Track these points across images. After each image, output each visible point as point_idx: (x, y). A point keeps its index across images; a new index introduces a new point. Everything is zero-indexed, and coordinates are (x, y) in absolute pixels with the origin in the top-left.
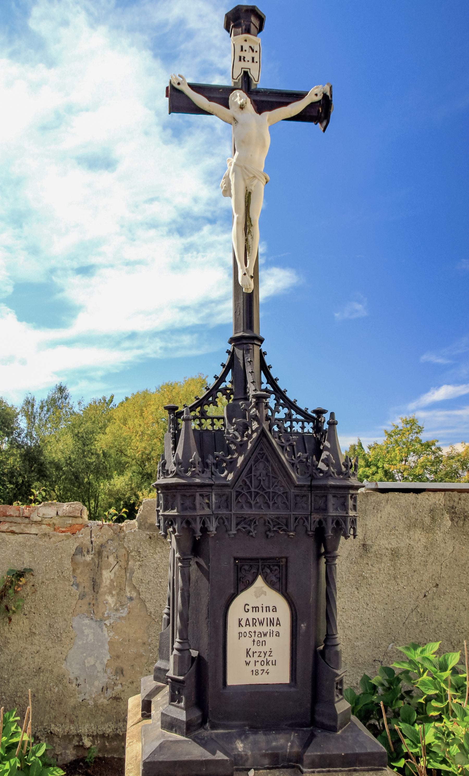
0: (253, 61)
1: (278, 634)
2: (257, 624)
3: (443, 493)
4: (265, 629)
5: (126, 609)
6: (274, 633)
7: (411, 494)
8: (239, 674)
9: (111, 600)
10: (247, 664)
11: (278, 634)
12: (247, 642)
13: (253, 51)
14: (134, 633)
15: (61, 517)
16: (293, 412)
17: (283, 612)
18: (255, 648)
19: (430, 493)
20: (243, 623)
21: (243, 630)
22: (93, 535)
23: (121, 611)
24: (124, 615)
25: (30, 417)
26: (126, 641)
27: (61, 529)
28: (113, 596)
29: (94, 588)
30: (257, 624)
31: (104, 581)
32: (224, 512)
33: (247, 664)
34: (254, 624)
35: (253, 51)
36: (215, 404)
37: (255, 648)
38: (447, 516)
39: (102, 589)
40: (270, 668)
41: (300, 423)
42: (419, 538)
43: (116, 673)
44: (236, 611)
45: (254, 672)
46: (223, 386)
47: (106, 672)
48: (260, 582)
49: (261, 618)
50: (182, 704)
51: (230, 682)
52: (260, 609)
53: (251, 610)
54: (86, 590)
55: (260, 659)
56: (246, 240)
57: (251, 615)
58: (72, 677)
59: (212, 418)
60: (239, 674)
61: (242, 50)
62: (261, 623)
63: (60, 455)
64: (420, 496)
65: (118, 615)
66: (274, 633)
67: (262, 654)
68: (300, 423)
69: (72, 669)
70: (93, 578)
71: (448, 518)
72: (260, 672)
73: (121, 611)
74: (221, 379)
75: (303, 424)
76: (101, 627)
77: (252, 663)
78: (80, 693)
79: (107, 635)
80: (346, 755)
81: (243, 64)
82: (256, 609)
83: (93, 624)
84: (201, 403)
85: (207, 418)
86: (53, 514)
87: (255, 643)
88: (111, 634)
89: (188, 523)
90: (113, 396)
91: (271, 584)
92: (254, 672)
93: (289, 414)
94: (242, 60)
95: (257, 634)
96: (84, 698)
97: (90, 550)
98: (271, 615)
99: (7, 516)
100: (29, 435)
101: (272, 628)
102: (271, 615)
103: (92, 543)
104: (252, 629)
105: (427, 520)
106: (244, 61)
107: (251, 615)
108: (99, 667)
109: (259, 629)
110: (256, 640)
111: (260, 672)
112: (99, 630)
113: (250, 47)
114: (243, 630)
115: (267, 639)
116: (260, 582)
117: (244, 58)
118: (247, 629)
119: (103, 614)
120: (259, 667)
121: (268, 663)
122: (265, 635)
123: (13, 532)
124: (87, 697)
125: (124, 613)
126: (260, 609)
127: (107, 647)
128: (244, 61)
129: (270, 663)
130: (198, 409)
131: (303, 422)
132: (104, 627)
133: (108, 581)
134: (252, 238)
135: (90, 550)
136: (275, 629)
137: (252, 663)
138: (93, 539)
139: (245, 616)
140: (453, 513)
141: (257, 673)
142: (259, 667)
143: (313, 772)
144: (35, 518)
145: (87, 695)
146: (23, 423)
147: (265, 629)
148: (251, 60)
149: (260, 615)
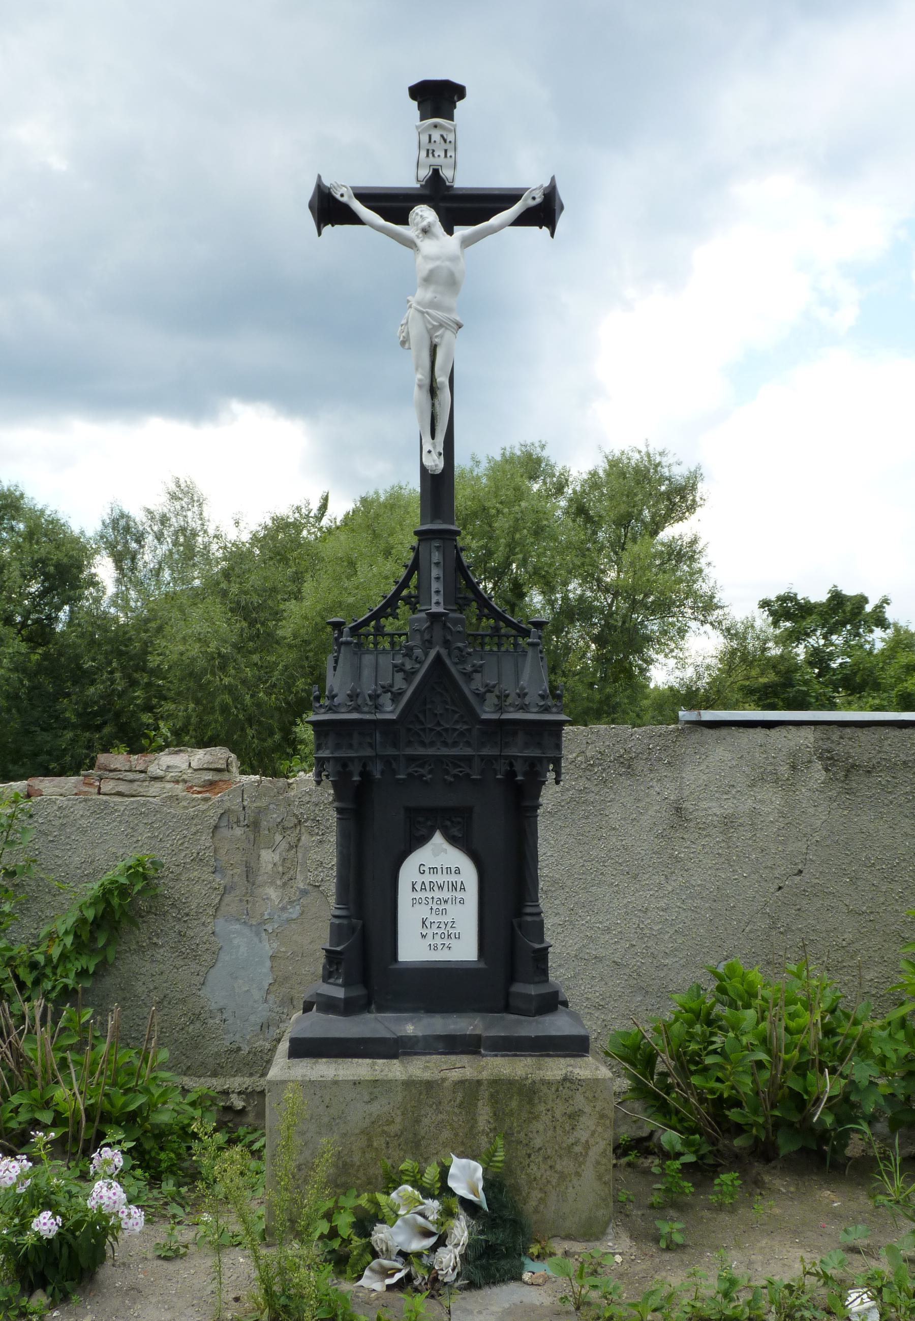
0: (446, 156)
1: (462, 901)
2: (436, 888)
3: (813, 727)
4: (445, 895)
5: (298, 907)
6: (458, 900)
7: (758, 730)
8: (414, 947)
9: (272, 893)
10: (424, 936)
11: (462, 901)
12: (423, 911)
13: (445, 141)
14: (310, 943)
15: (195, 770)
16: (502, 624)
17: (469, 875)
18: (433, 918)
19: (790, 727)
20: (418, 887)
21: (417, 895)
22: (245, 797)
23: (291, 910)
24: (294, 916)
25: (124, 559)
26: (298, 956)
27: (195, 788)
28: (277, 887)
29: (247, 876)
30: (436, 888)
31: (264, 865)
32: (391, 751)
33: (424, 936)
34: (432, 889)
35: (445, 141)
36: (396, 617)
37: (433, 918)
38: (818, 765)
39: (260, 878)
40: (453, 942)
41: (512, 640)
42: (771, 800)
43: (282, 1004)
44: (410, 872)
45: (432, 947)
46: (405, 593)
47: (266, 1001)
48: (438, 839)
49: (440, 882)
50: (340, 981)
51: (401, 958)
52: (440, 871)
53: (427, 871)
54: (236, 879)
55: (440, 931)
56: (433, 405)
57: (427, 878)
58: (214, 1006)
59: (392, 635)
60: (414, 947)
61: (430, 141)
62: (441, 888)
63: (195, 649)
64: (774, 733)
65: (285, 916)
66: (458, 900)
67: (442, 926)
68: (512, 640)
69: (214, 995)
70: (246, 862)
71: (820, 767)
72: (440, 947)
73: (291, 910)
74: (404, 584)
75: (515, 639)
76: (258, 934)
77: (430, 936)
78: (228, 1032)
79: (268, 947)
80: (536, 1037)
81: (432, 161)
82: (433, 870)
83: (246, 931)
84: (377, 615)
85: (384, 635)
86: (185, 766)
87: (433, 911)
88: (275, 945)
89: (345, 765)
90: (327, 496)
91: (452, 840)
92: (432, 947)
93: (495, 627)
94: (431, 155)
95: (435, 900)
96: (233, 1039)
97: (242, 819)
98: (453, 878)
99: (111, 771)
100: (120, 600)
101: (454, 894)
102: (453, 878)
103: (244, 808)
104: (430, 895)
105: (784, 770)
106: (433, 155)
107: (427, 878)
108: (257, 995)
109: (437, 894)
110: (434, 908)
111: (440, 947)
112: (256, 940)
113: (442, 136)
114: (417, 895)
115: (448, 906)
116: (438, 839)
117: (433, 151)
118: (423, 895)
119: (262, 915)
120: (438, 941)
121: (449, 936)
122: (446, 902)
123: (119, 794)
124: (237, 1038)
125: (294, 912)
126: (440, 871)
127: (268, 963)
128: (433, 155)
129: (452, 936)
130: (373, 623)
131: (515, 637)
132: (264, 934)
133: (270, 866)
134: (440, 404)
135: (242, 819)
136: (459, 895)
137: (430, 936)
138: (245, 803)
139: (419, 879)
140: (829, 759)
141: (436, 948)
142: (438, 941)
143: (496, 1056)
144: (154, 770)
145: (238, 1035)
146: (104, 570)
147: (445, 895)
148: (442, 154)
149: (439, 879)
